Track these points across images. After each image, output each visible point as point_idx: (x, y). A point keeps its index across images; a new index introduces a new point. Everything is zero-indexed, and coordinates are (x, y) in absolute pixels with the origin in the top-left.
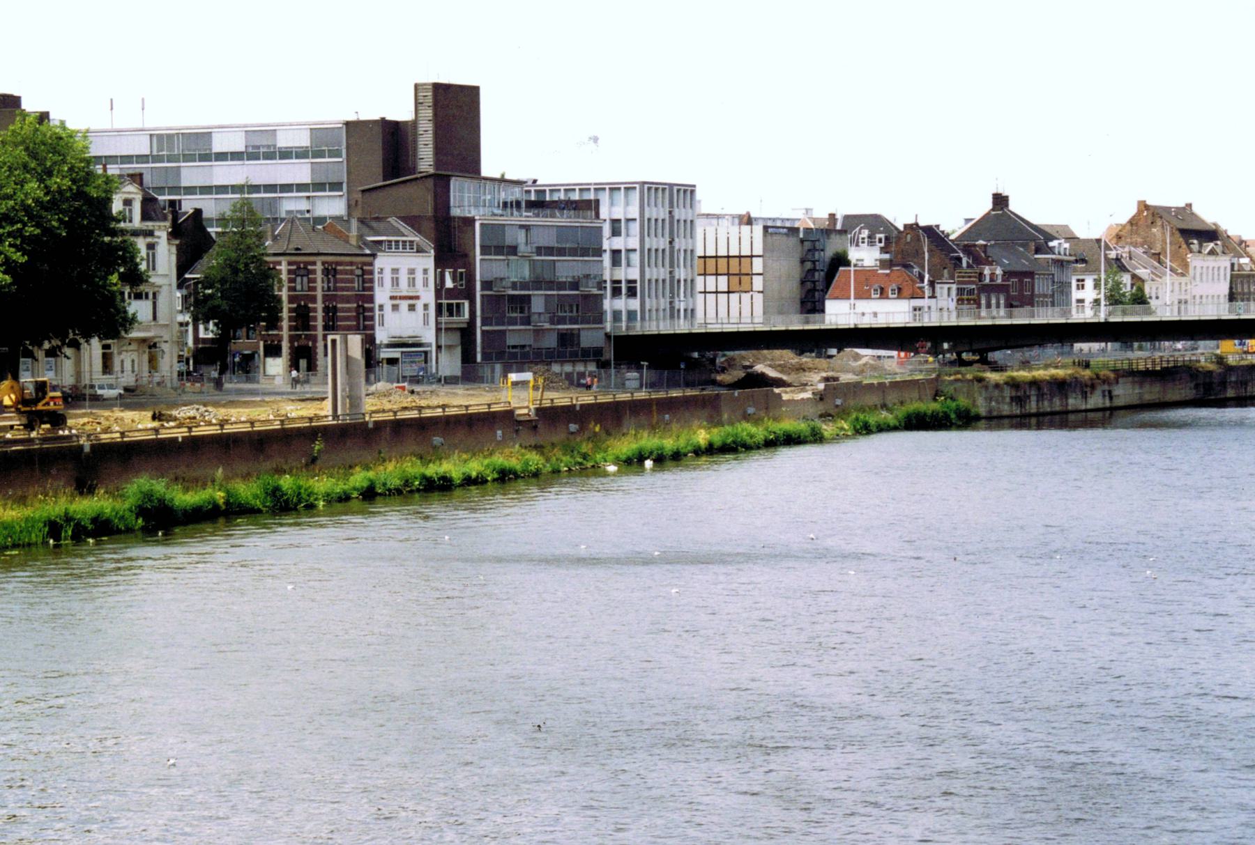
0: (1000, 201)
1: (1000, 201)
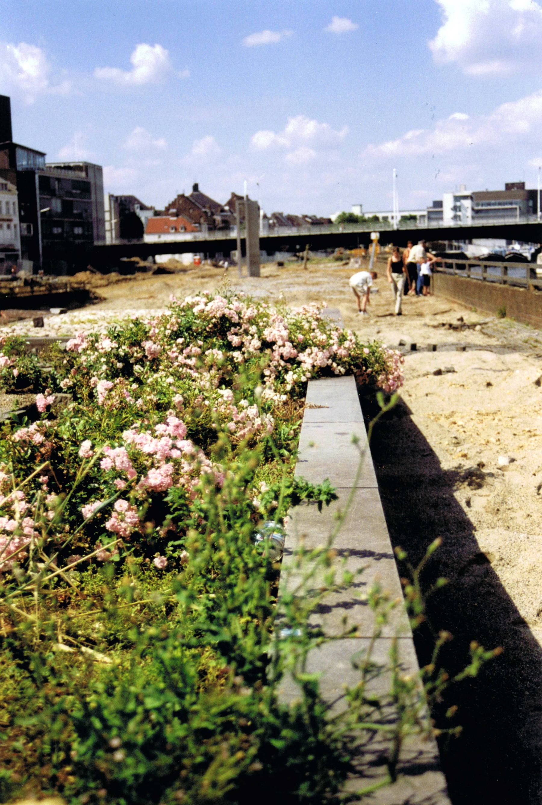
0: (196, 187)
1: (196, 187)
